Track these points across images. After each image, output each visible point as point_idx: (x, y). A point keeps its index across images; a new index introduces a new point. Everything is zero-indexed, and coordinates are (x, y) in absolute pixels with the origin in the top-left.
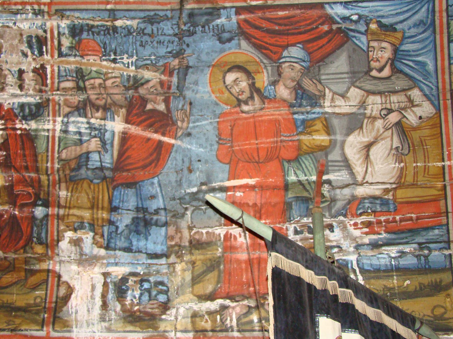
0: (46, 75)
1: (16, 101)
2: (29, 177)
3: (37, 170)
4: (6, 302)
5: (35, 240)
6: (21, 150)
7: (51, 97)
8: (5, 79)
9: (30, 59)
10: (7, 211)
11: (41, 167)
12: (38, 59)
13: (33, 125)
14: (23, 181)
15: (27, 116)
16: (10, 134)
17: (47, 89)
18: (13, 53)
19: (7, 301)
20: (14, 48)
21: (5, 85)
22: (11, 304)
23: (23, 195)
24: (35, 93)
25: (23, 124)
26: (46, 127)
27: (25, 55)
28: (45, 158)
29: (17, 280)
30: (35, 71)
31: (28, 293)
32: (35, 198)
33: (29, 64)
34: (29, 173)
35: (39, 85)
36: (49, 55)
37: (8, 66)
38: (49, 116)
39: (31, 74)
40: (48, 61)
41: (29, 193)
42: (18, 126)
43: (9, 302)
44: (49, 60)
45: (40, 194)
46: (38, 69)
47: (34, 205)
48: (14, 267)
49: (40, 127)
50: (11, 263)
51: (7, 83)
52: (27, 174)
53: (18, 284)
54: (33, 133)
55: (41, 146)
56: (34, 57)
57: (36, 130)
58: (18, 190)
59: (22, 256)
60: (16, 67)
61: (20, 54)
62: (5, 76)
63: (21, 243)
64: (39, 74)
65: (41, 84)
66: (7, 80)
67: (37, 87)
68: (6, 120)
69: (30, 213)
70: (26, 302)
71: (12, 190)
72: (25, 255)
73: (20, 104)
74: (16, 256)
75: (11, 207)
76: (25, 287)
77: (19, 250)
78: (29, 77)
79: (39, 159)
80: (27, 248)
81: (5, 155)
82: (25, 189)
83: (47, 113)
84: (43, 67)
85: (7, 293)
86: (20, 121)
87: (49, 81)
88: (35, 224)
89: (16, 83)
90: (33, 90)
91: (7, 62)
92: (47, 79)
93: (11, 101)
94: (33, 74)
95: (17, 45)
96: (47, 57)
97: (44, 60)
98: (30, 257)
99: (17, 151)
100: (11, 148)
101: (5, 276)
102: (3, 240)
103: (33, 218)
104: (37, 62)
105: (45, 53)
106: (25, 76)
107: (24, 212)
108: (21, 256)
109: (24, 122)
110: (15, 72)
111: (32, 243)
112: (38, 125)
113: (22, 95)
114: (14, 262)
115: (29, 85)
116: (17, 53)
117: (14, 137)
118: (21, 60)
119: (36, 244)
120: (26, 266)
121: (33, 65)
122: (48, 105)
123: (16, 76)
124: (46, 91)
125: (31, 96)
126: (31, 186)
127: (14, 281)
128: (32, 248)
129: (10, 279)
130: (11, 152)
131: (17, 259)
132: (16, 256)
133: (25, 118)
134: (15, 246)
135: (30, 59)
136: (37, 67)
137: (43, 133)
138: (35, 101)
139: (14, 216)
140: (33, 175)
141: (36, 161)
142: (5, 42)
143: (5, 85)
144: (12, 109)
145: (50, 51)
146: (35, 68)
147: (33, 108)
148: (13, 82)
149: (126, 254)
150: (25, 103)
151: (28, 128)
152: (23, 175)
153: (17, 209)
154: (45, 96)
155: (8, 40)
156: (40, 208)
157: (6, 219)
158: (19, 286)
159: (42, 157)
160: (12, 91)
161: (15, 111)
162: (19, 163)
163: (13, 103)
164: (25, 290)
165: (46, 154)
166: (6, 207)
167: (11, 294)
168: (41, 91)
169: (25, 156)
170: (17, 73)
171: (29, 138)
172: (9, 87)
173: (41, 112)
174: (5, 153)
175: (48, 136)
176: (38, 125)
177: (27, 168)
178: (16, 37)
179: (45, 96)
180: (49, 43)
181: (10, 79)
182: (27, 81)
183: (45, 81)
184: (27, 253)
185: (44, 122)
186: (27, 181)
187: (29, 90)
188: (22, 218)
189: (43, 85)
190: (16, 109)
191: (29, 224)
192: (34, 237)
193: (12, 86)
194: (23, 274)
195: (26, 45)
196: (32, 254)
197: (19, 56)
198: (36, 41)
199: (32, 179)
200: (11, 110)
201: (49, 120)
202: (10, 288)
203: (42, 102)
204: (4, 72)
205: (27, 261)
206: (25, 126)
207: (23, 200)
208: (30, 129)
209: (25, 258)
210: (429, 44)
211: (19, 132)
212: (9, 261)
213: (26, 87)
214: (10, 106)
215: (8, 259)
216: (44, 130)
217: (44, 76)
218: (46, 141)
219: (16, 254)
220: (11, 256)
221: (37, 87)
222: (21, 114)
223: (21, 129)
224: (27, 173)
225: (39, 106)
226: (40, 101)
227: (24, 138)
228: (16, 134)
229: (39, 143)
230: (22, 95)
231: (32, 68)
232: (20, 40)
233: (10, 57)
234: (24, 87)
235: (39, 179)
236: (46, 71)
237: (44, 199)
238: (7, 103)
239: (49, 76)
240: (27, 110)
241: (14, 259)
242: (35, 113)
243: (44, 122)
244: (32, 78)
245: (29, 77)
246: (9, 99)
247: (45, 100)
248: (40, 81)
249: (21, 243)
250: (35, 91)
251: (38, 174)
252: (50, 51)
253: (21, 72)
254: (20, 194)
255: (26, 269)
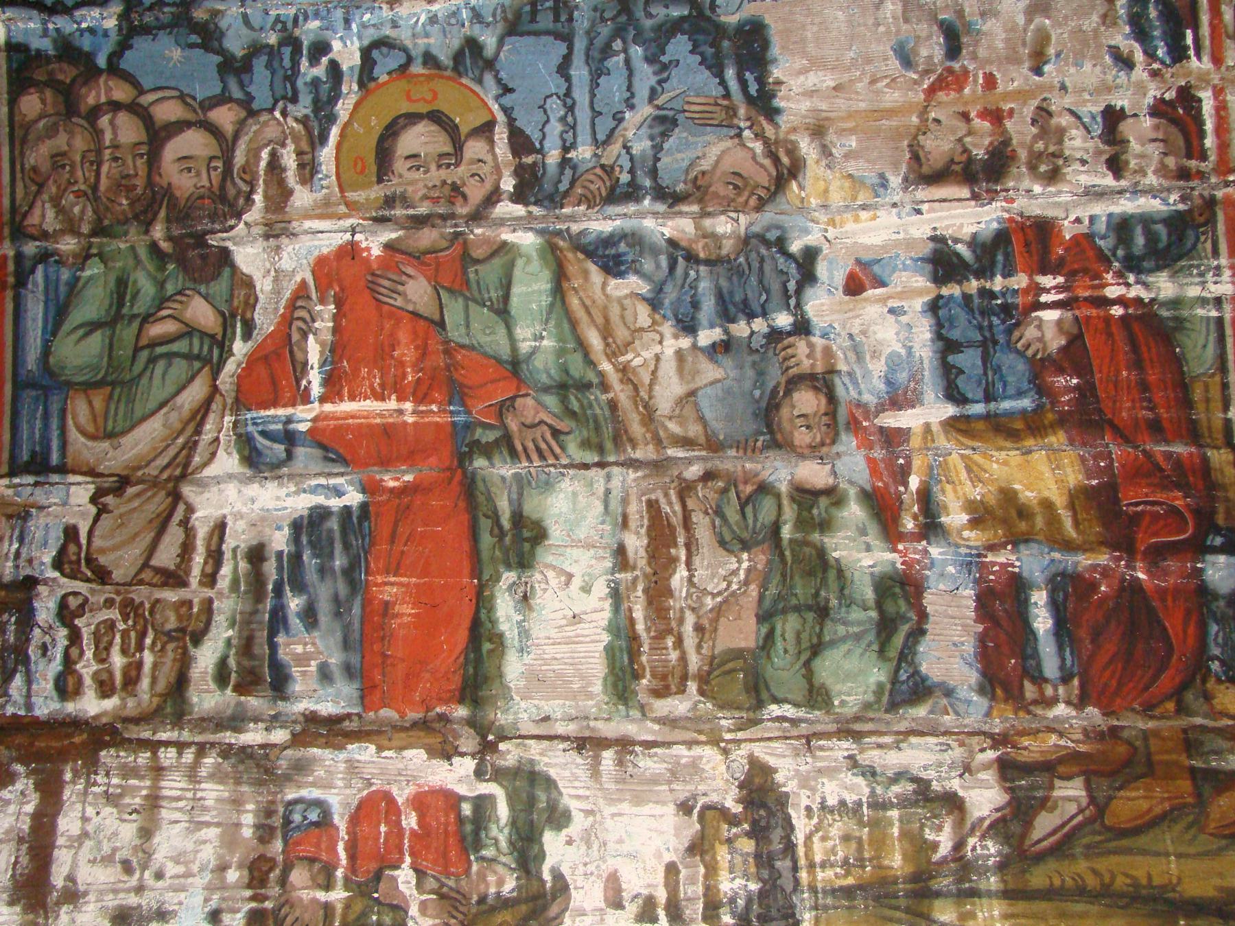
0: (1200, 122)
1: (1101, 209)
2: (1168, 456)
3: (1193, 433)
4: (1144, 882)
5: (1215, 666)
6: (1128, 369)
7: (1219, 194)
8: (1060, 142)
9: (1140, 73)
10: (1105, 572)
11: (1205, 424)
12: (1167, 73)
13: (1164, 286)
14: (1148, 471)
15: (1141, 259)
16: (1088, 318)
17: (1205, 166)
18: (1084, 57)
19: (1150, 877)
20: (1085, 43)
21: (1061, 162)
22: (1163, 888)
23: (1155, 517)
24: (1165, 183)
25: (1128, 285)
26: (1215, 290)
27: (1125, 62)
28: (1215, 393)
29: (1167, 806)
30: (1159, 109)
31: (1220, 849)
32: (1198, 526)
33: (1138, 91)
34: (1167, 442)
35: (1176, 156)
36: (1205, 58)
37: (1068, 101)
38: (1216, 253)
39: (1148, 122)
40: (1204, 78)
41: (1174, 511)
42: (1113, 292)
43: (1156, 881)
44: (1208, 73)
45: (1213, 512)
46: (1170, 103)
47: (1199, 548)
48: (1150, 764)
49: (1193, 292)
50: (1135, 749)
51: (1067, 153)
52: (1163, 448)
53: (1174, 821)
54: (1165, 313)
55: (1198, 353)
56: (1155, 66)
57: (1176, 303)
58: (1133, 499)
59: (1170, 723)
60: (1095, 103)
61: (1108, 59)
62: (1061, 132)
63: (1167, 680)
64: (1175, 121)
65: (1183, 152)
66: (1067, 143)
67: (1171, 162)
68: (1071, 275)
69: (1189, 576)
70: (1217, 882)
71: (1117, 501)
72: (1184, 722)
73: (1115, 220)
74: (1151, 724)
75: (1119, 559)
76: (1202, 830)
77: (1162, 702)
78: (1141, 133)
79: (1197, 394)
80: (1189, 696)
81: (1077, 388)
82: (1159, 497)
83: (1209, 245)
84: (1187, 97)
85: (1144, 852)
86: (1119, 274)
87: (1209, 142)
88: (1210, 610)
89: (1098, 153)
90: (1155, 172)
91: (1063, 88)
92: (1202, 134)
93: (1084, 213)
94: (1156, 121)
95: (1095, 31)
96: (1198, 65)
97: (1189, 74)
98: (1203, 728)
99: (1118, 372)
100: (1095, 363)
101: (1122, 793)
102: (1104, 669)
103: (1203, 592)
104: (1164, 81)
105: (1191, 52)
106: (1126, 127)
107: (1166, 573)
108: (1168, 725)
109: (1131, 278)
110: (1093, 118)
111: (1204, 681)
112: (1181, 286)
113: (1121, 192)
114: (1147, 747)
115: (1142, 156)
116: (1096, 58)
117: (1101, 326)
118: (1109, 77)
119: (1219, 681)
120: (1190, 757)
121: (1153, 92)
122: (1211, 221)
123: (1097, 129)
124: (1201, 175)
125: (1152, 192)
126: (1177, 486)
127: (1158, 810)
128: (1208, 697)
129: (1145, 805)
130: (1097, 376)
131: (1156, 733)
132: (1151, 724)
133: (1133, 264)
134: (1146, 688)
135: (1140, 73)
136: (1167, 96)
137: (1200, 312)
138: (1164, 208)
139: (1136, 584)
140: (1180, 449)
141: (1188, 404)
142: (1057, 24)
143: (1061, 162)
144: (1089, 237)
145: (1207, 43)
146: (1162, 100)
147: (1161, 229)
148: (1087, 151)
149: (597, 667)
150: (1132, 216)
151: (1146, 296)
152: (1144, 451)
153: (1139, 564)
154: (1199, 189)
155: (1066, 17)
156: (1222, 559)
157: (1105, 598)
158: (1178, 827)
159: (1207, 388)
160: (1085, 179)
161: (1101, 243)
162: (1127, 410)
163: (1092, 219)
164: (1204, 842)
165: (1217, 378)
166: (1103, 559)
167: (1157, 854)
168: (1184, 174)
169: (1144, 386)
170: (1099, 119)
171: (1154, 330)
172: (1077, 166)
173: (1189, 244)
174: (1075, 381)
175: (1220, 321)
176: (1181, 286)
177: (1156, 429)
178: (1093, 7)
179: (1199, 189)
180: (1205, 18)
181: (1078, 143)
182: (1135, 146)
183: (1195, 143)
184: (1190, 713)
185: (1201, 275)
186: (1162, 470)
187: (1145, 175)
188: (1162, 593)
189: (1189, 156)
190: (1103, 238)
191: (1188, 612)
192: (1212, 659)
193: (1083, 162)
194: (1185, 785)
195: (1127, 29)
196: (1205, 716)
197: (1104, 66)
198: (1161, 14)
199: (1178, 462)
200: (1085, 241)
201: (1218, 268)
202: (1151, 834)
203: (1190, 211)
204: (1054, 121)
205: (1190, 742)
206: (1135, 292)
207: (1156, 534)
208: (1153, 300)
209: (1185, 731)
210: (501, 222)
211: (1117, 311)
212: (1129, 743)
213: (1133, 164)
214: (1083, 228)
215: (1125, 734)
216: (1203, 302)
217: (1192, 128)
218: (1212, 337)
219: (1152, 717)
220: (1134, 723)
221: (1171, 162)
222: (1120, 253)
223: (1121, 301)
224: (1158, 442)
225: (1178, 223)
226: (1181, 207)
227: (1136, 327)
228: (1108, 319)
229: (1188, 343)
230: (1121, 192)
231: (1149, 100)
232: (1104, 17)
233: (1072, 70)
234: (1127, 163)
235: (1205, 460)
236: (1200, 109)
237: (1228, 529)
238: (1072, 218)
239: (1209, 126)
240: (1140, 240)
241: (1146, 735)
242: (1169, 246)
243: (1201, 275)
244: (1154, 136)
245: (1141, 133)
246: (1076, 205)
247: (1198, 202)
248: (1181, 142)
249: (1167, 680)
250: (1164, 176)
251: (1201, 446)
252: (1207, 43)
253: (1113, 117)
254: (1143, 512)
255: (1193, 771)
